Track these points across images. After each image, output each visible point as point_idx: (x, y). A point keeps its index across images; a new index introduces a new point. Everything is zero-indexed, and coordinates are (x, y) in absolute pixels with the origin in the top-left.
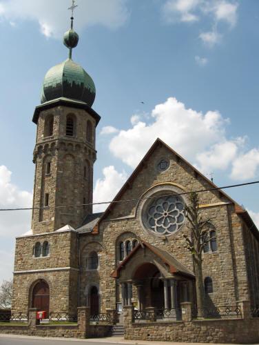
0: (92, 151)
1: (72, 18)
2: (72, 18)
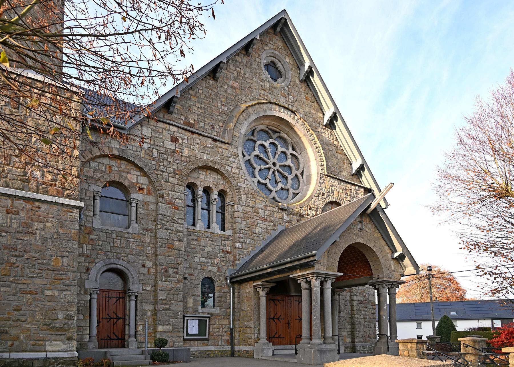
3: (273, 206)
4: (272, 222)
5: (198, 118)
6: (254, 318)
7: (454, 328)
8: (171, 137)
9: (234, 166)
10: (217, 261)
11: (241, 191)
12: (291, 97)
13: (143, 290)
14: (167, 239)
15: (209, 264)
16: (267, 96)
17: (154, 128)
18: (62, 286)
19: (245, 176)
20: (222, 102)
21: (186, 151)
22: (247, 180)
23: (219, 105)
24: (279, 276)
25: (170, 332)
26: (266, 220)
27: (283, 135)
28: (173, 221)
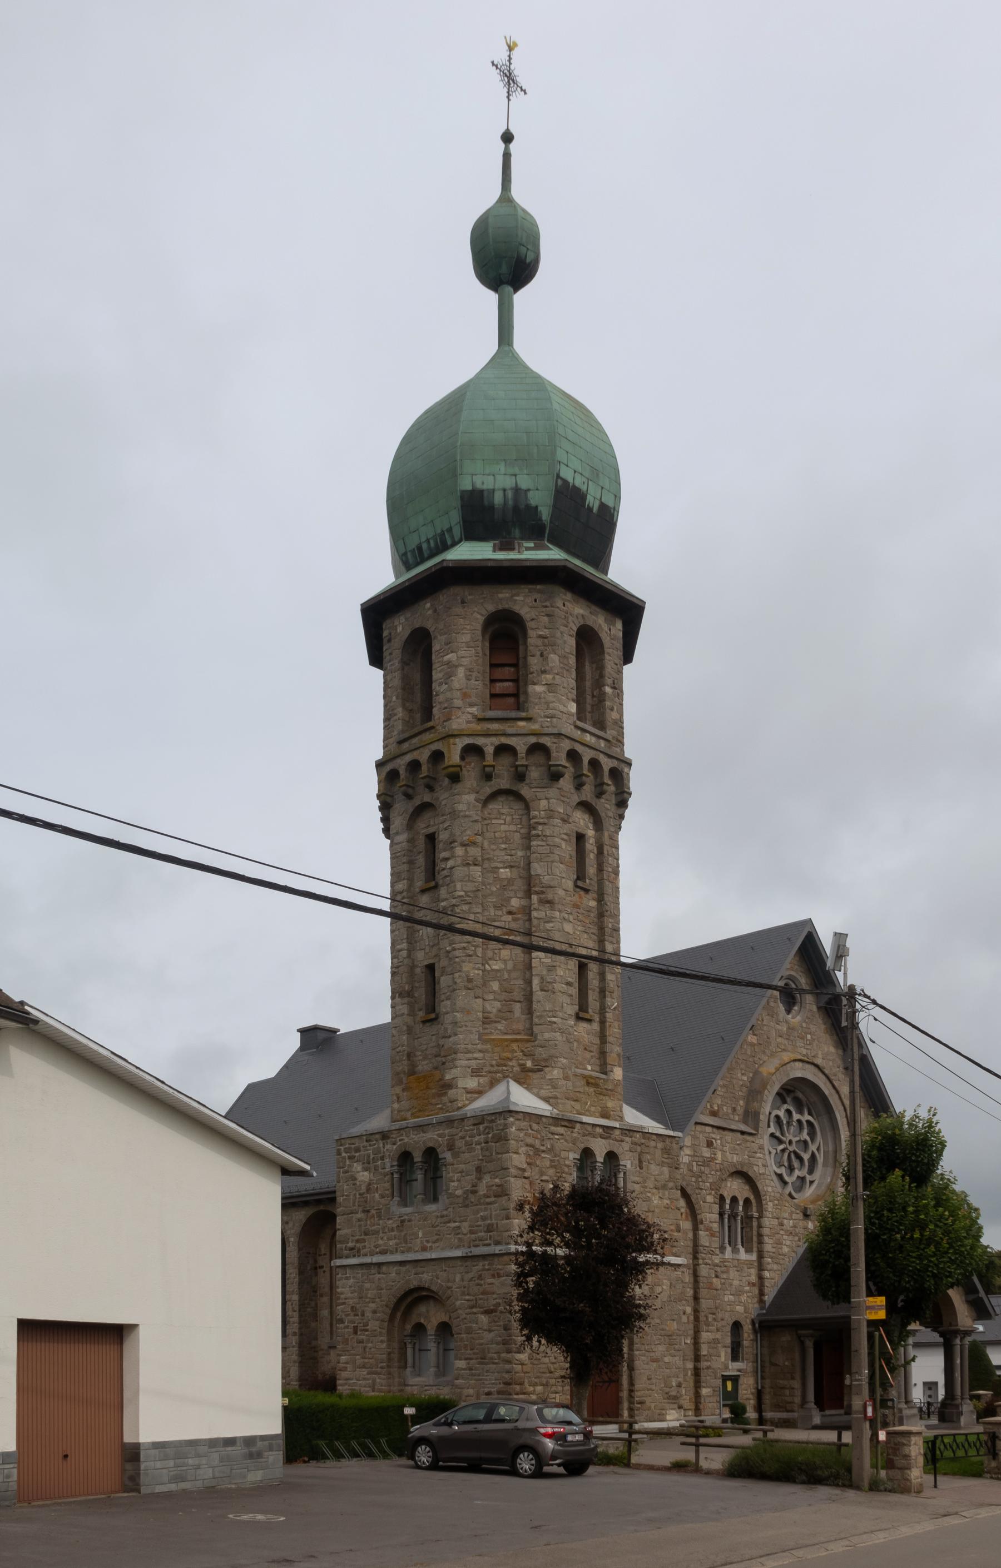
0: (607, 764)
1: (507, 138)
2: (507, 138)
3: (798, 1212)
4: (796, 1235)
5: (722, 1101)
6: (798, 1375)
7: (995, 1374)
8: (707, 1140)
9: (760, 1164)
10: (744, 1298)
11: (768, 1197)
12: (809, 1037)
13: (685, 1343)
14: (706, 1277)
15: (736, 1303)
16: (785, 1045)
17: (693, 1133)
18: (353, 1317)
19: (770, 1176)
20: (741, 1069)
21: (719, 1155)
22: (772, 1180)
23: (739, 1075)
24: (958, 1361)
25: (710, 1396)
26: (791, 1233)
27: (800, 1095)
28: (711, 1252)
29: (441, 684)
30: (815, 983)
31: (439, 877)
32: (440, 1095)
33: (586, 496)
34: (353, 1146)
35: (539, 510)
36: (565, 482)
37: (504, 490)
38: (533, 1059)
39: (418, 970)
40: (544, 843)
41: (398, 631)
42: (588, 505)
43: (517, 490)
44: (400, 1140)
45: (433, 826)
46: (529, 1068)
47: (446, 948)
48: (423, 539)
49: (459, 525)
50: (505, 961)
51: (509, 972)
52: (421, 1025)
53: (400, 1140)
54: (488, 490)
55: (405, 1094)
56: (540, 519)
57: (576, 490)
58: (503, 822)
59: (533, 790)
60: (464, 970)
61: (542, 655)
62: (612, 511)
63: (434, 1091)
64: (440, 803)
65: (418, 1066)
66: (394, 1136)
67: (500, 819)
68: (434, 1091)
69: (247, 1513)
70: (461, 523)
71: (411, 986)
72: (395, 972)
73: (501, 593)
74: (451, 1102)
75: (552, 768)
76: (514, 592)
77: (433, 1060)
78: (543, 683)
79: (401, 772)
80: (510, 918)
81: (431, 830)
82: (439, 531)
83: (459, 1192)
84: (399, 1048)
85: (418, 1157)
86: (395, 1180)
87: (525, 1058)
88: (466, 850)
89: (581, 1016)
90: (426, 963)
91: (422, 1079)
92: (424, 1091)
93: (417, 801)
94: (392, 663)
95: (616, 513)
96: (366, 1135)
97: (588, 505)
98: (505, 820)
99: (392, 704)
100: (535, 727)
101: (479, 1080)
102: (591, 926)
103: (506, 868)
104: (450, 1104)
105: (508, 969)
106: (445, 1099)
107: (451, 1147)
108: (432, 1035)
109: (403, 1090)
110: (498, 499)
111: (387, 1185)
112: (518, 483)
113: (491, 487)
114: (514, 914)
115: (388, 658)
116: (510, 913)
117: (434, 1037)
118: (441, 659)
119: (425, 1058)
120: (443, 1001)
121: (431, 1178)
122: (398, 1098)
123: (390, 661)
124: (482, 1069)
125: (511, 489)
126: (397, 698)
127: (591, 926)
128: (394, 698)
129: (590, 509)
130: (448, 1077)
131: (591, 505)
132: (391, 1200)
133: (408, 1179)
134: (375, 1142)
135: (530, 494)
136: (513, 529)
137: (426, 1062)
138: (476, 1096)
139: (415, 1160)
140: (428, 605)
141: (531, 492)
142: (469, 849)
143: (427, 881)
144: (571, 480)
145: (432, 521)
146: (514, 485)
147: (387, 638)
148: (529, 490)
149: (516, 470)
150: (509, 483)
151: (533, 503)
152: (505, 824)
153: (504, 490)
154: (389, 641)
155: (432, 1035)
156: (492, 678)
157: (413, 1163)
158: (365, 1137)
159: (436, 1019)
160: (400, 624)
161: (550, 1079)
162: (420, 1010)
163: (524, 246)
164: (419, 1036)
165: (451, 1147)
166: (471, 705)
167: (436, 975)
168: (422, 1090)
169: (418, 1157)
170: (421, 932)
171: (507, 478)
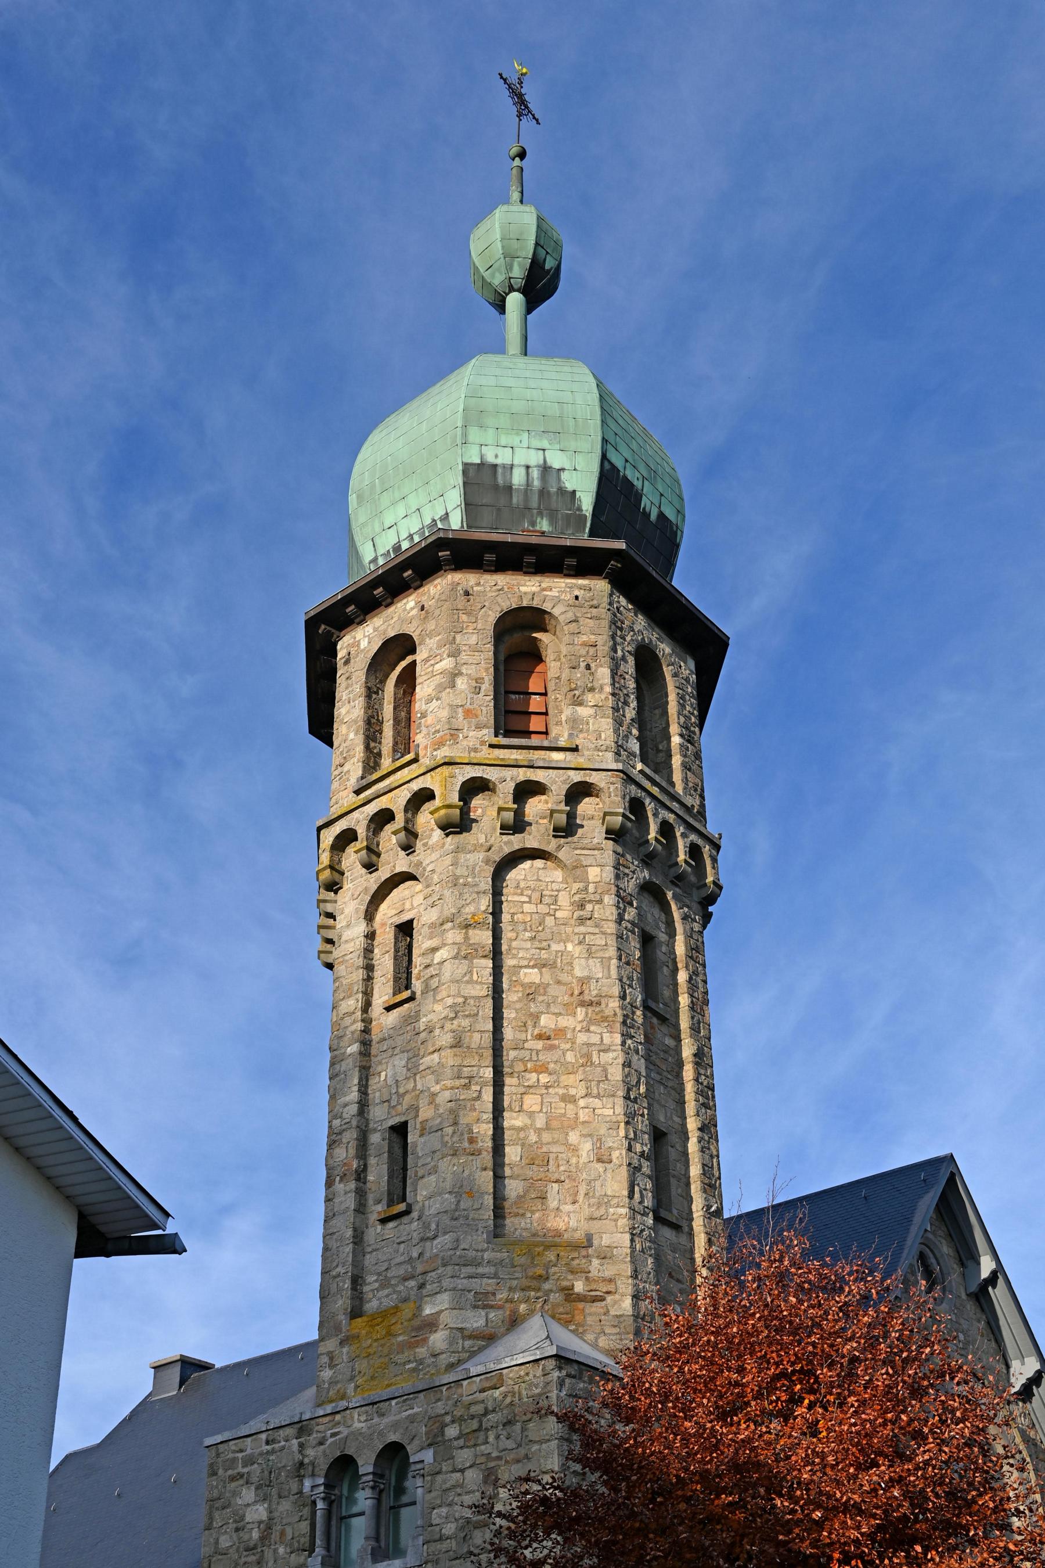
29: (429, 701)
30: (957, 1248)
31: (417, 985)
32: (412, 1345)
33: (641, 497)
34: (240, 1455)
35: (577, 496)
36: (613, 467)
37: (528, 467)
38: (587, 1278)
39: (375, 1138)
40: (597, 930)
41: (362, 647)
42: (644, 509)
43: (545, 469)
44: (333, 1435)
45: (410, 910)
46: (578, 1294)
47: (429, 1089)
48: (404, 535)
49: (459, 509)
50: (531, 1115)
51: (539, 1131)
52: (379, 1227)
53: (333, 1435)
54: (504, 466)
55: (345, 1350)
56: (580, 509)
57: (628, 483)
58: (525, 899)
59: (578, 852)
60: (462, 1122)
61: (588, 667)
62: (675, 529)
63: (400, 1338)
64: (424, 869)
65: (370, 1301)
66: (321, 1428)
67: (522, 894)
68: (400, 1338)
69: (668, 738)
70: (463, 506)
71: (362, 1163)
72: (335, 1142)
73: (525, 585)
74: (435, 1356)
75: (608, 818)
76: (544, 585)
77: (401, 1288)
78: (591, 704)
79: (359, 831)
80: (539, 1045)
81: (405, 917)
82: (428, 521)
83: (449, 1529)
84: (338, 1270)
85: (366, 1466)
86: (319, 1513)
87: (570, 1277)
88: (466, 933)
89: (662, 1215)
90: (392, 1122)
91: (380, 1320)
92: (382, 1342)
93: (384, 873)
94: (350, 689)
95: (679, 533)
96: (267, 1430)
97: (644, 509)
98: (530, 897)
99: (348, 743)
100: (579, 760)
101: (487, 1314)
102: (669, 1076)
103: (533, 967)
104: (433, 1360)
105: (538, 1126)
106: (422, 1352)
107: (436, 1440)
108: (399, 1243)
109: (342, 1343)
110: (518, 478)
111: (304, 1527)
112: (548, 460)
113: (508, 461)
114: (549, 1038)
115: (344, 685)
116: (540, 1037)
117: (402, 1245)
118: (431, 669)
119: (385, 1284)
120: (422, 1177)
121: (391, 1508)
122: (331, 1359)
123: (347, 688)
124: (494, 1294)
125: (538, 466)
126: (356, 734)
127: (669, 1076)
128: (352, 736)
129: (646, 515)
130: (428, 1311)
131: (647, 509)
132: (310, 1556)
133: (344, 1514)
134: (283, 1443)
135: (564, 476)
136: (539, 520)
137: (386, 1292)
138: (483, 1343)
139: (361, 1471)
140: (412, 604)
141: (566, 472)
142: (471, 932)
143: (396, 992)
144: (620, 468)
145: (419, 510)
146: (541, 462)
147: (344, 660)
148: (563, 469)
149: (545, 444)
150: (535, 459)
151: (569, 486)
152: (530, 902)
153: (528, 467)
154: (347, 662)
155: (399, 1243)
156: (507, 709)
157: (356, 1476)
158: (264, 1436)
159: (407, 1212)
160: (365, 636)
161: (617, 1316)
162: (379, 1202)
163: (542, 247)
164: (374, 1247)
165: (436, 1440)
166: (479, 727)
167: (409, 1141)
168: (376, 1340)
169: (366, 1466)
170: (383, 1074)
171: (533, 452)
